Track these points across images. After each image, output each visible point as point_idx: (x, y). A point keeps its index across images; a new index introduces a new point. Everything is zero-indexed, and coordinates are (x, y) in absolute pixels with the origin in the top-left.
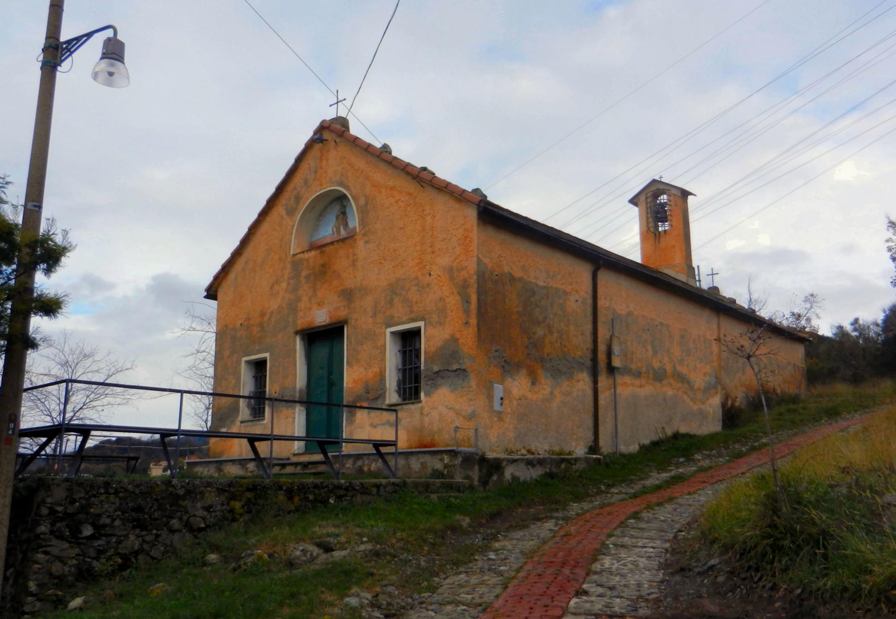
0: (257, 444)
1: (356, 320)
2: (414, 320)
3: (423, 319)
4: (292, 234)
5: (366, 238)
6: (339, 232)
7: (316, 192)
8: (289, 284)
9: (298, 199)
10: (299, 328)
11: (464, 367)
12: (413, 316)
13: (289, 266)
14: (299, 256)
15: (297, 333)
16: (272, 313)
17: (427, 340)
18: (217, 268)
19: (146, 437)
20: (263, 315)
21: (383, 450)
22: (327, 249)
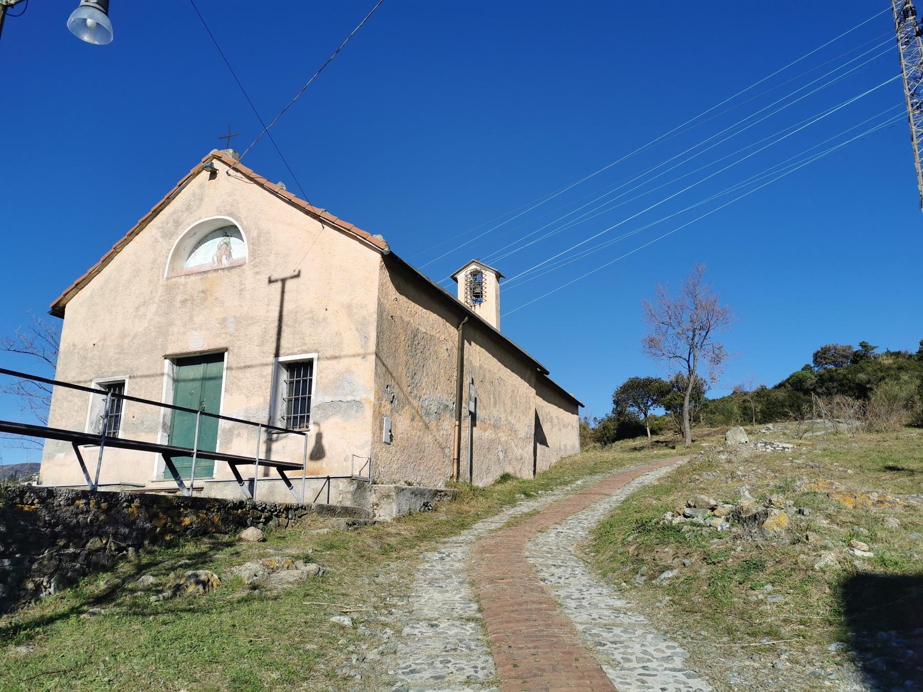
0: (174, 459)
1: (240, 348)
2: (306, 352)
3: (316, 351)
4: (167, 257)
5: (257, 270)
6: (220, 261)
7: (189, 224)
8: (159, 307)
9: (177, 223)
10: (169, 352)
11: (358, 399)
12: (305, 348)
13: (160, 291)
14: (173, 280)
15: (166, 357)
16: (135, 336)
17: (320, 371)
18: (309, 218)
19: (284, 389)
20: (123, 336)
21: (288, 473)
22: (210, 275)
